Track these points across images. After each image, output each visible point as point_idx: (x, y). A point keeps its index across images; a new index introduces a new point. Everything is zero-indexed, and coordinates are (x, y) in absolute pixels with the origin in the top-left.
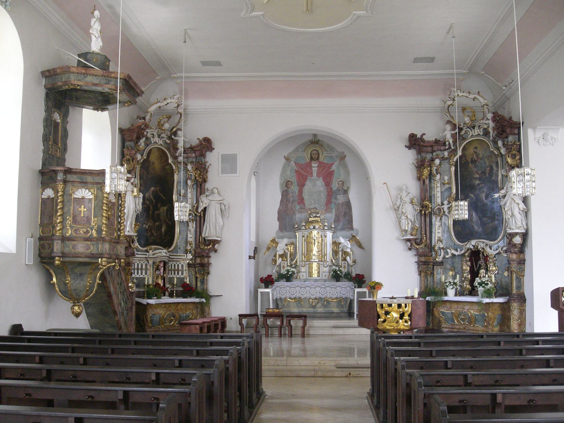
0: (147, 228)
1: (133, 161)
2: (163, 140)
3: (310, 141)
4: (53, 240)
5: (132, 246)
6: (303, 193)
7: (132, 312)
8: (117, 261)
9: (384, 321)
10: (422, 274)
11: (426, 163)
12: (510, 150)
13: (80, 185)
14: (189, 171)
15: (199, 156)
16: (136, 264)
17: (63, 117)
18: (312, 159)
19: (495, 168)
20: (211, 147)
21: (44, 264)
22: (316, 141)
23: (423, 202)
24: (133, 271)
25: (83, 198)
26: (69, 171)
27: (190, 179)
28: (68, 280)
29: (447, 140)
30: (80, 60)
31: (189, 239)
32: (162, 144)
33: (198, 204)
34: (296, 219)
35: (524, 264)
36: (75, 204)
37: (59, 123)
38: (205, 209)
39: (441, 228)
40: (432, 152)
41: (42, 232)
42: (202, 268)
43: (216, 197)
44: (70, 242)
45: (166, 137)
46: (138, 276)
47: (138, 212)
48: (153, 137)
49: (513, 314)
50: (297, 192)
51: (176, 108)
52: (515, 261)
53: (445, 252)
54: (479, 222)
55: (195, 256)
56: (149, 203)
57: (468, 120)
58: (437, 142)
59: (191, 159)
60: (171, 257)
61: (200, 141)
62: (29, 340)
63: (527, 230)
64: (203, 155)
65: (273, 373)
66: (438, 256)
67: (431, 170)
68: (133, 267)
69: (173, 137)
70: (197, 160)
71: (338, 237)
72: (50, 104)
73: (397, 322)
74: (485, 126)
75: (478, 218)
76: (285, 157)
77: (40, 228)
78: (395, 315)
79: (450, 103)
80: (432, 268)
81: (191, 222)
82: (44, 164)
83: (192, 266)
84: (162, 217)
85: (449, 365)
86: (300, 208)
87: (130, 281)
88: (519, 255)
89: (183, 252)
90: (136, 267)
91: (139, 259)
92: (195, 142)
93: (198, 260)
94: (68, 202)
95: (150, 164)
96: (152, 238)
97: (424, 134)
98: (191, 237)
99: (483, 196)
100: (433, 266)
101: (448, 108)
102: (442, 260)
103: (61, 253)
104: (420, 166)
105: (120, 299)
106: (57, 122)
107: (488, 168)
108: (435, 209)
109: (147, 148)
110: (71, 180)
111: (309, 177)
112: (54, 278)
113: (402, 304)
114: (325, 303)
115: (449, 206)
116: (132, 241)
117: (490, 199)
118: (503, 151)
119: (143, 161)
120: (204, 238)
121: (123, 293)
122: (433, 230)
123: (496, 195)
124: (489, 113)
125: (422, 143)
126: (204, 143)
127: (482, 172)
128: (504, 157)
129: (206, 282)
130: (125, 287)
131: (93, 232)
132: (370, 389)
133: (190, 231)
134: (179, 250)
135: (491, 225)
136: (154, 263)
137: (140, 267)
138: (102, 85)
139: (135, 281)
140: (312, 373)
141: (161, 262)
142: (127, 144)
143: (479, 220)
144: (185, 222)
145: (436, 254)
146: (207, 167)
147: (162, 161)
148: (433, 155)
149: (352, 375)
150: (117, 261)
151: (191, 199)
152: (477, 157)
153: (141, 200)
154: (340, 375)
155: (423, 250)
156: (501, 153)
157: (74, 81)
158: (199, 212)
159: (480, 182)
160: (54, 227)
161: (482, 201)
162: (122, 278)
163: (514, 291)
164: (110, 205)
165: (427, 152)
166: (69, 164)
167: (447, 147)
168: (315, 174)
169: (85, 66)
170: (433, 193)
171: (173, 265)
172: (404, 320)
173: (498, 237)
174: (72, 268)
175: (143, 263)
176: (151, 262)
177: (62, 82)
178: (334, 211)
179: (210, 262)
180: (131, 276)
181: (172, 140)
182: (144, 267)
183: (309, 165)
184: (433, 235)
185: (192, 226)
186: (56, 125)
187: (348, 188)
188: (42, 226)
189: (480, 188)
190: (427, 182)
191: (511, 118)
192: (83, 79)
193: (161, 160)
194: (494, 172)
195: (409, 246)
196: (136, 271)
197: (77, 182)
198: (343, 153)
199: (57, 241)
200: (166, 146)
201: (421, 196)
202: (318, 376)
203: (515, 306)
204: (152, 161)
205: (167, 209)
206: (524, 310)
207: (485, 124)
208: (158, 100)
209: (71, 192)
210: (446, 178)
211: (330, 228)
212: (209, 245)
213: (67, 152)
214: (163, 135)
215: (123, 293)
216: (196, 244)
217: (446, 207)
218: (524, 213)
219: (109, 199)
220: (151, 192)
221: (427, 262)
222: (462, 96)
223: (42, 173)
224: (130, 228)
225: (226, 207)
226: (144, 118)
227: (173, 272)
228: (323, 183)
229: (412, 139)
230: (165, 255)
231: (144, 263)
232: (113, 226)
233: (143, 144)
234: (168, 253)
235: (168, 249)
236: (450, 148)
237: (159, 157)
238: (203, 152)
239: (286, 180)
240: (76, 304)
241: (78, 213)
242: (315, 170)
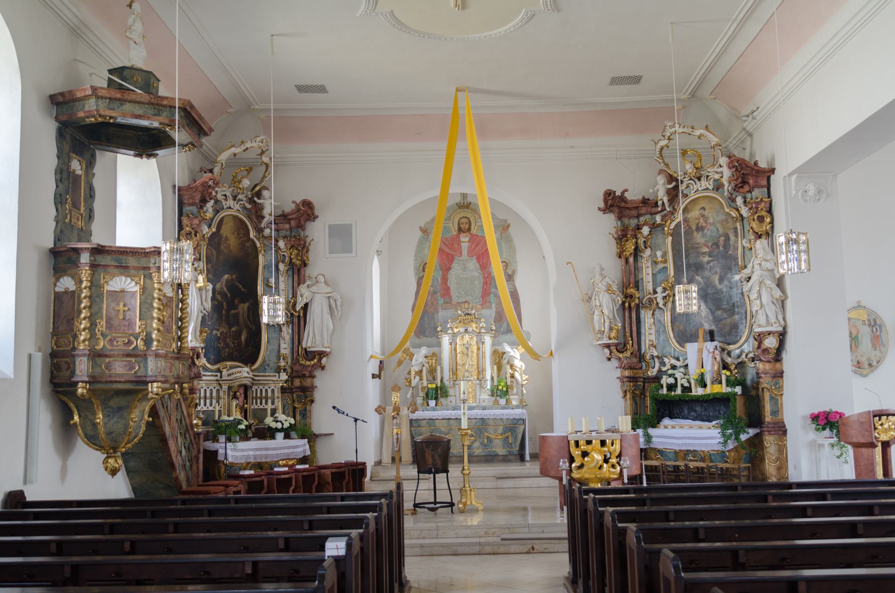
0: (219, 335)
1: (196, 235)
2: (240, 204)
3: (457, 204)
4: (74, 356)
5: (197, 362)
6: (449, 281)
7: (197, 463)
8: (176, 386)
9: (581, 466)
10: (628, 396)
11: (630, 233)
12: (755, 210)
13: (116, 271)
14: (280, 249)
15: (296, 228)
16: (202, 391)
17: (87, 167)
18: (460, 230)
19: (732, 237)
20: (313, 214)
21: (58, 395)
22: (465, 204)
23: (626, 289)
24: (198, 401)
25: (123, 291)
26: (99, 250)
27: (283, 262)
28: (99, 418)
29: (659, 198)
30: (111, 79)
31: (283, 351)
32: (240, 210)
33: (296, 298)
34: (439, 318)
35: (782, 377)
36: (110, 300)
37: (81, 176)
38: (306, 307)
39: (653, 327)
40: (638, 217)
41: (56, 344)
42: (302, 394)
43: (322, 288)
44: (102, 359)
45: (245, 199)
46: (205, 408)
47: (205, 312)
48: (226, 200)
49: (769, 453)
50: (439, 279)
51: (259, 157)
52: (767, 373)
53: (660, 363)
54: (711, 318)
55: (292, 378)
56: (221, 297)
57: (691, 168)
58: (645, 201)
59: (283, 232)
60: (255, 378)
61: (297, 205)
62: (37, 516)
63: (784, 328)
64: (301, 227)
65: (418, 550)
66: (651, 369)
67: (636, 243)
68: (198, 395)
69: (256, 199)
70: (293, 234)
71: (500, 344)
72: (67, 147)
73: (601, 467)
74: (717, 176)
75: (709, 312)
76: (420, 227)
77: (52, 338)
78: (598, 457)
79: (664, 143)
80: (641, 387)
81: (285, 325)
82: (57, 239)
83: (288, 391)
84: (241, 317)
85: (702, 535)
86: (444, 303)
87: (194, 417)
88: (773, 364)
89: (273, 370)
90: (202, 394)
91: (206, 382)
92: (289, 208)
93: (297, 383)
94: (98, 296)
95: (221, 239)
96: (227, 350)
97: (626, 190)
98: (285, 348)
99: (716, 279)
100: (644, 382)
101: (661, 151)
102: (657, 374)
103: (88, 376)
104: (622, 237)
105: (180, 444)
106: (77, 175)
107: (722, 238)
108: (645, 300)
109: (217, 216)
110: (102, 264)
111: (456, 257)
112: (75, 415)
113: (607, 441)
114: (485, 441)
115: (664, 295)
116: (197, 355)
117: (726, 282)
118: (744, 211)
119: (211, 235)
120: (306, 349)
121: (185, 434)
122: (643, 331)
123: (737, 277)
124: (722, 156)
125: (623, 204)
126: (303, 208)
127: (713, 245)
128: (745, 221)
129: (308, 414)
130: (187, 426)
131: (138, 342)
132: (569, 573)
133: (284, 339)
134: (267, 367)
135: (728, 321)
136: (230, 388)
137: (208, 395)
138: (148, 117)
139: (202, 416)
140: (477, 549)
141: (240, 386)
142: (186, 209)
143: (710, 314)
144: (276, 326)
145: (648, 365)
146: (307, 244)
147: (241, 235)
148: (639, 220)
149: (537, 550)
150: (176, 386)
151: (284, 292)
152: (705, 221)
153: (210, 294)
154: (518, 551)
155: (629, 360)
156: (741, 215)
157: (104, 111)
158: (298, 310)
159: (710, 259)
160: (75, 337)
161: (715, 287)
162: (182, 412)
163: (768, 418)
164: (165, 301)
165: (630, 217)
166: (98, 238)
167: (659, 209)
168: (465, 252)
169: (121, 88)
170: (640, 277)
171: (259, 390)
172: (610, 464)
173: (740, 338)
174: (105, 400)
175: (213, 389)
176: (225, 387)
177: (85, 112)
178: (494, 305)
179: (315, 385)
180: (195, 408)
181: (254, 204)
182: (214, 394)
183: (456, 240)
184: (643, 338)
185: (287, 332)
186: (77, 179)
187: (514, 272)
188: (56, 335)
189: (711, 268)
190: (631, 260)
191: (756, 164)
192: (118, 107)
193: (238, 234)
194: (731, 242)
195: (608, 354)
196: (202, 401)
197: (113, 266)
198: (506, 221)
199: (81, 358)
200: (245, 212)
201: (623, 282)
202: (486, 552)
203: (769, 441)
204: (225, 235)
205: (248, 307)
206: (785, 446)
207: (717, 172)
208: (232, 144)
209: (102, 282)
210: (659, 254)
211: (489, 330)
212: (312, 360)
213: (93, 221)
214: (240, 197)
215: (185, 434)
216: (293, 359)
217: (660, 296)
218: (780, 303)
219: (164, 292)
220: (224, 281)
221: (636, 378)
222: (683, 132)
223: (55, 253)
224: (193, 336)
225: (338, 303)
226: (211, 171)
227: (259, 401)
228: (477, 265)
229: (610, 198)
230: (246, 375)
231: (215, 388)
232: (169, 333)
233: (210, 210)
234: (251, 373)
235: (250, 367)
236: (664, 209)
237: (236, 229)
238: (302, 222)
239: (423, 261)
240: (112, 455)
241: (114, 313)
242: (465, 246)
